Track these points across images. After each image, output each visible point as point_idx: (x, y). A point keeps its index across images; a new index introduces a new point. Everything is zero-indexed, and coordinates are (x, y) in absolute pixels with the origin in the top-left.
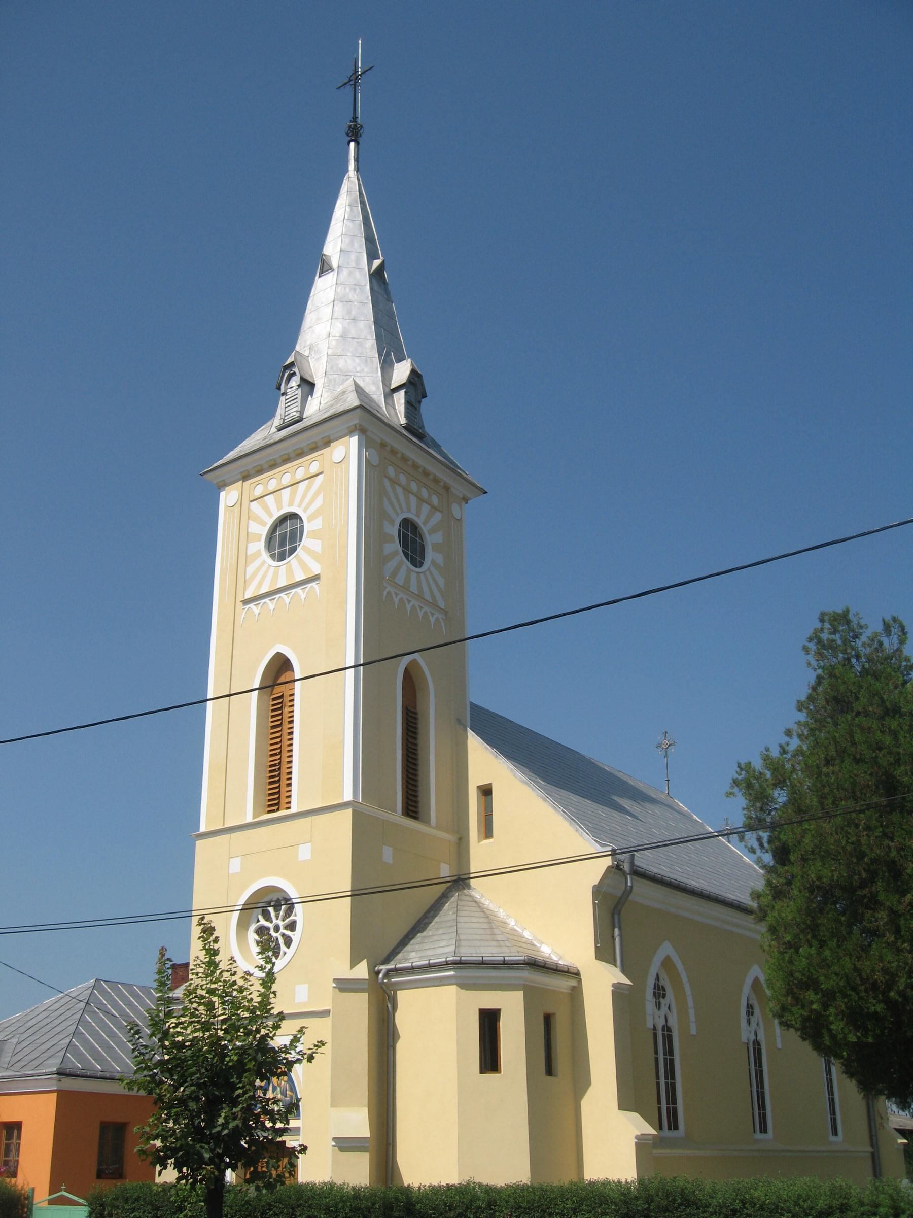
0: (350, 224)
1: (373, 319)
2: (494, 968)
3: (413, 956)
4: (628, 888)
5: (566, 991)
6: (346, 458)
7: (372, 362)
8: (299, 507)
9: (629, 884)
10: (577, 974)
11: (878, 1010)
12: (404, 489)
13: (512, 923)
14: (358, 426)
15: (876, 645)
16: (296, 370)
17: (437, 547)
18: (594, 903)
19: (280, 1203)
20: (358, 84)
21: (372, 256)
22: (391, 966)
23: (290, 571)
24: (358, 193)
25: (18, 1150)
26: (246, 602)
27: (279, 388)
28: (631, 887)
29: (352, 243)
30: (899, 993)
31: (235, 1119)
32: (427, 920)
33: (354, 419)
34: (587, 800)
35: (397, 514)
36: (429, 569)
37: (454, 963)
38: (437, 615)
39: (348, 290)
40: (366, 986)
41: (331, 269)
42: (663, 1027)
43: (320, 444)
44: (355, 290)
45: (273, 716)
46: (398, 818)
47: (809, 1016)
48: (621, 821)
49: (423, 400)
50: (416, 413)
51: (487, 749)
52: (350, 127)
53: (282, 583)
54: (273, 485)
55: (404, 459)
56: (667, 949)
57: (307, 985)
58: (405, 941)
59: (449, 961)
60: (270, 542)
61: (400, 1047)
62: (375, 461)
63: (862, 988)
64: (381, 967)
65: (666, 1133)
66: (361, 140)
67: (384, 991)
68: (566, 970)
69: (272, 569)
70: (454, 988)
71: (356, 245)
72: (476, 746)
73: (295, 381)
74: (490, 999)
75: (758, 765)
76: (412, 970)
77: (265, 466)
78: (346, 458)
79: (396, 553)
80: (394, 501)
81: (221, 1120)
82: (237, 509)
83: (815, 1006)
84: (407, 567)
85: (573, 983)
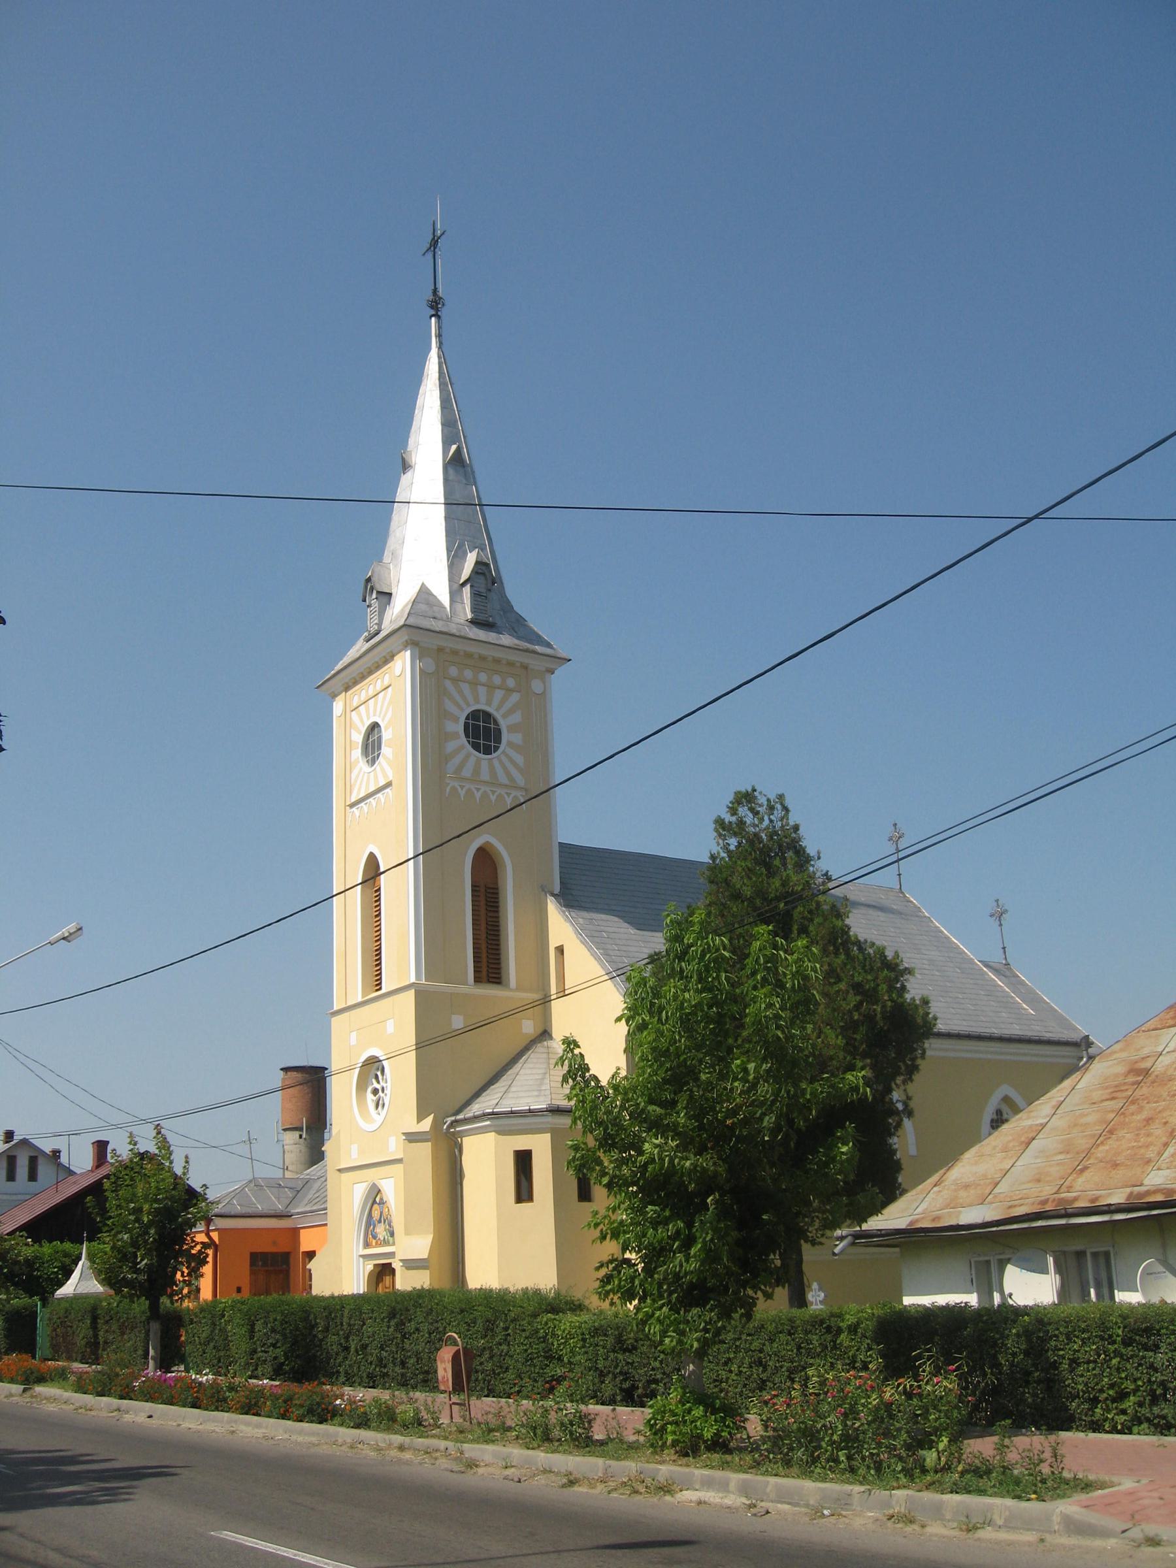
3: (476, 1108)
12: (470, 683)
26: (352, 805)
27: (364, 600)
36: (504, 752)
37: (489, 1114)
46: (469, 987)
53: (372, 789)
58: (477, 1095)
62: (431, 668)
66: (443, 313)
70: (491, 1136)
74: (522, 1142)
82: (343, 718)
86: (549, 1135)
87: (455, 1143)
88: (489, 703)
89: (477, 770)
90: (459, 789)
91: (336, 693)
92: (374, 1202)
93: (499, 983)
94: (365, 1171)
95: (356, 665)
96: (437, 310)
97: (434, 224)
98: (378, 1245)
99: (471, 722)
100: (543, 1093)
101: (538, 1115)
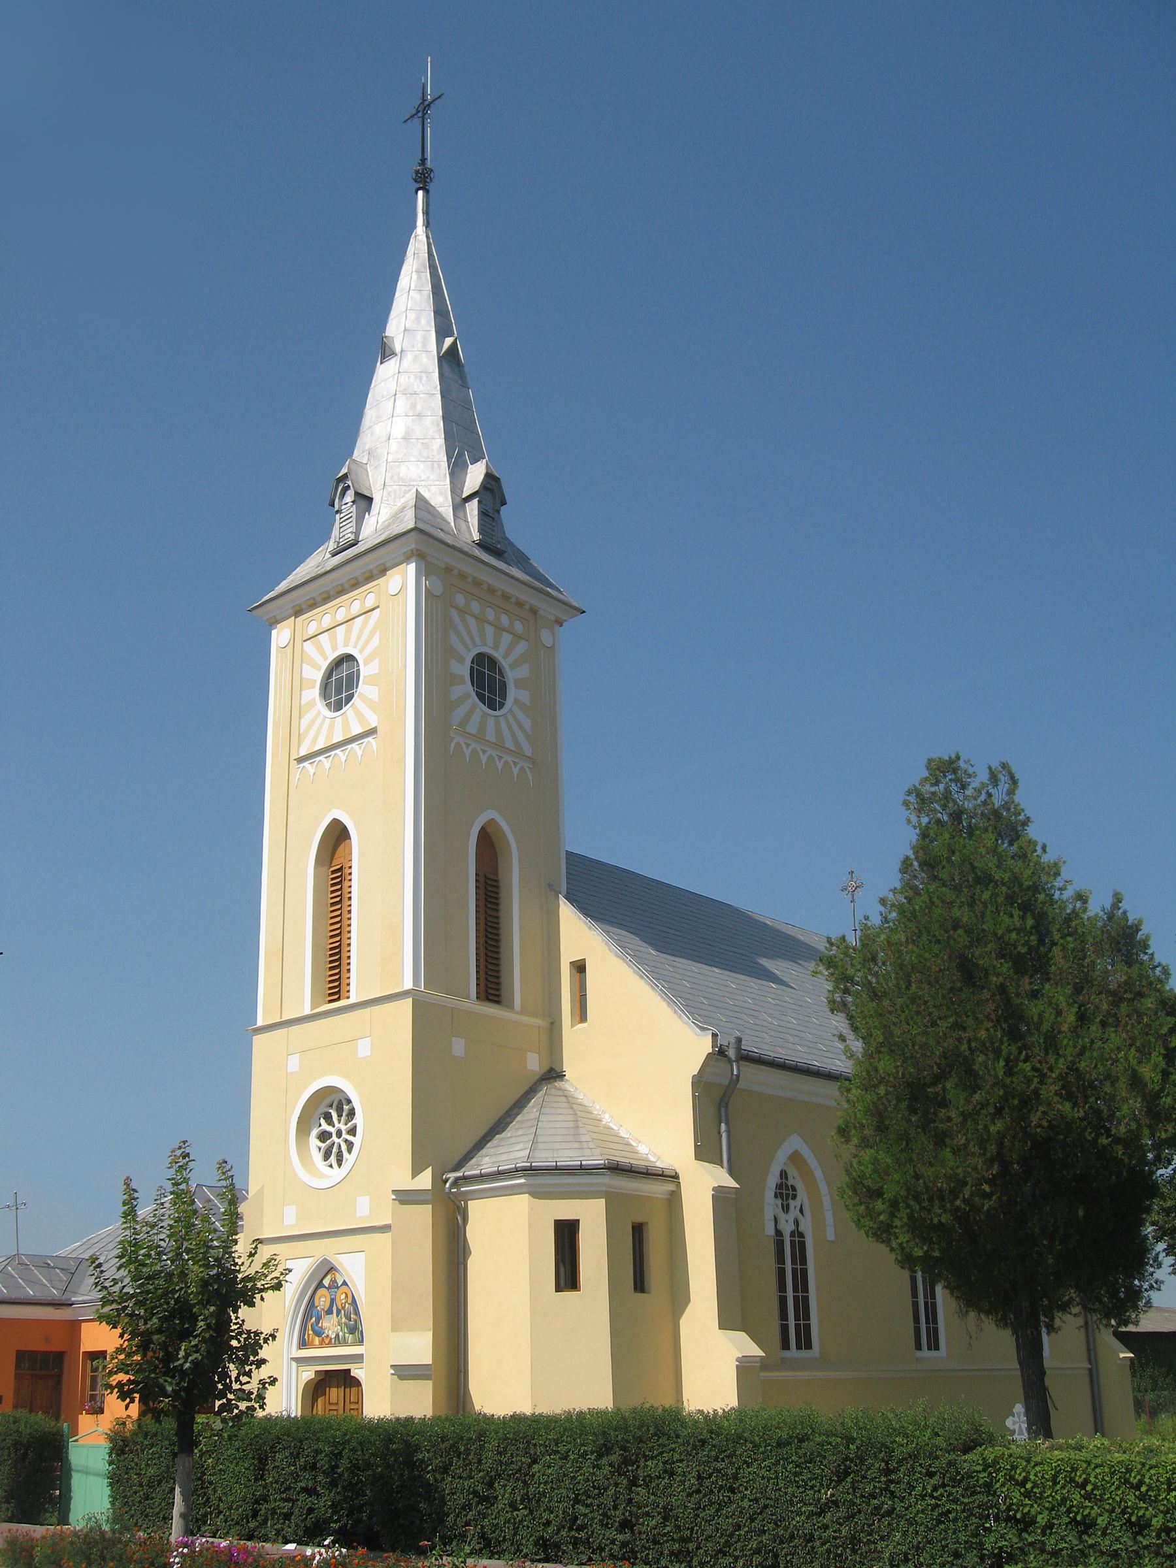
1: (441, 414)
2: (570, 1174)
3: (486, 1162)
4: (734, 1077)
5: (663, 1196)
6: (403, 587)
7: (439, 467)
8: (355, 647)
9: (735, 1073)
10: (676, 1177)
11: (943, 1221)
13: (606, 1118)
14: (414, 552)
15: (983, 797)
16: (350, 483)
17: (521, 684)
18: (693, 1095)
19: (289, 1436)
20: (426, 116)
21: (442, 332)
22: (459, 1174)
23: (346, 724)
24: (427, 255)
26: (301, 760)
28: (738, 1076)
29: (418, 319)
33: (411, 544)
34: (715, 969)
37: (525, 1169)
39: (412, 379)
40: (429, 1197)
41: (393, 354)
42: (792, 1234)
45: (332, 892)
46: (472, 1004)
48: (759, 992)
49: (502, 508)
50: (494, 524)
51: (580, 919)
52: (417, 172)
54: (327, 621)
55: (477, 583)
56: (795, 1143)
57: (368, 1197)
59: (519, 1167)
60: (325, 688)
62: (439, 591)
63: (926, 1197)
65: (793, 1352)
66: (431, 187)
67: (453, 1201)
68: (661, 1173)
69: (328, 721)
70: (525, 1197)
71: (423, 321)
72: (567, 914)
73: (349, 497)
74: (566, 1209)
76: (481, 1178)
77: (319, 599)
79: (467, 696)
80: (464, 633)
81: (182, 1354)
82: (289, 650)
84: (482, 711)
85: (671, 1187)
87: (458, 1207)
89: (482, 728)
91: (278, 618)
92: (320, 1285)
94: (310, 1243)
95: (366, 559)
98: (322, 1345)
99: (475, 667)
100: (585, 1145)
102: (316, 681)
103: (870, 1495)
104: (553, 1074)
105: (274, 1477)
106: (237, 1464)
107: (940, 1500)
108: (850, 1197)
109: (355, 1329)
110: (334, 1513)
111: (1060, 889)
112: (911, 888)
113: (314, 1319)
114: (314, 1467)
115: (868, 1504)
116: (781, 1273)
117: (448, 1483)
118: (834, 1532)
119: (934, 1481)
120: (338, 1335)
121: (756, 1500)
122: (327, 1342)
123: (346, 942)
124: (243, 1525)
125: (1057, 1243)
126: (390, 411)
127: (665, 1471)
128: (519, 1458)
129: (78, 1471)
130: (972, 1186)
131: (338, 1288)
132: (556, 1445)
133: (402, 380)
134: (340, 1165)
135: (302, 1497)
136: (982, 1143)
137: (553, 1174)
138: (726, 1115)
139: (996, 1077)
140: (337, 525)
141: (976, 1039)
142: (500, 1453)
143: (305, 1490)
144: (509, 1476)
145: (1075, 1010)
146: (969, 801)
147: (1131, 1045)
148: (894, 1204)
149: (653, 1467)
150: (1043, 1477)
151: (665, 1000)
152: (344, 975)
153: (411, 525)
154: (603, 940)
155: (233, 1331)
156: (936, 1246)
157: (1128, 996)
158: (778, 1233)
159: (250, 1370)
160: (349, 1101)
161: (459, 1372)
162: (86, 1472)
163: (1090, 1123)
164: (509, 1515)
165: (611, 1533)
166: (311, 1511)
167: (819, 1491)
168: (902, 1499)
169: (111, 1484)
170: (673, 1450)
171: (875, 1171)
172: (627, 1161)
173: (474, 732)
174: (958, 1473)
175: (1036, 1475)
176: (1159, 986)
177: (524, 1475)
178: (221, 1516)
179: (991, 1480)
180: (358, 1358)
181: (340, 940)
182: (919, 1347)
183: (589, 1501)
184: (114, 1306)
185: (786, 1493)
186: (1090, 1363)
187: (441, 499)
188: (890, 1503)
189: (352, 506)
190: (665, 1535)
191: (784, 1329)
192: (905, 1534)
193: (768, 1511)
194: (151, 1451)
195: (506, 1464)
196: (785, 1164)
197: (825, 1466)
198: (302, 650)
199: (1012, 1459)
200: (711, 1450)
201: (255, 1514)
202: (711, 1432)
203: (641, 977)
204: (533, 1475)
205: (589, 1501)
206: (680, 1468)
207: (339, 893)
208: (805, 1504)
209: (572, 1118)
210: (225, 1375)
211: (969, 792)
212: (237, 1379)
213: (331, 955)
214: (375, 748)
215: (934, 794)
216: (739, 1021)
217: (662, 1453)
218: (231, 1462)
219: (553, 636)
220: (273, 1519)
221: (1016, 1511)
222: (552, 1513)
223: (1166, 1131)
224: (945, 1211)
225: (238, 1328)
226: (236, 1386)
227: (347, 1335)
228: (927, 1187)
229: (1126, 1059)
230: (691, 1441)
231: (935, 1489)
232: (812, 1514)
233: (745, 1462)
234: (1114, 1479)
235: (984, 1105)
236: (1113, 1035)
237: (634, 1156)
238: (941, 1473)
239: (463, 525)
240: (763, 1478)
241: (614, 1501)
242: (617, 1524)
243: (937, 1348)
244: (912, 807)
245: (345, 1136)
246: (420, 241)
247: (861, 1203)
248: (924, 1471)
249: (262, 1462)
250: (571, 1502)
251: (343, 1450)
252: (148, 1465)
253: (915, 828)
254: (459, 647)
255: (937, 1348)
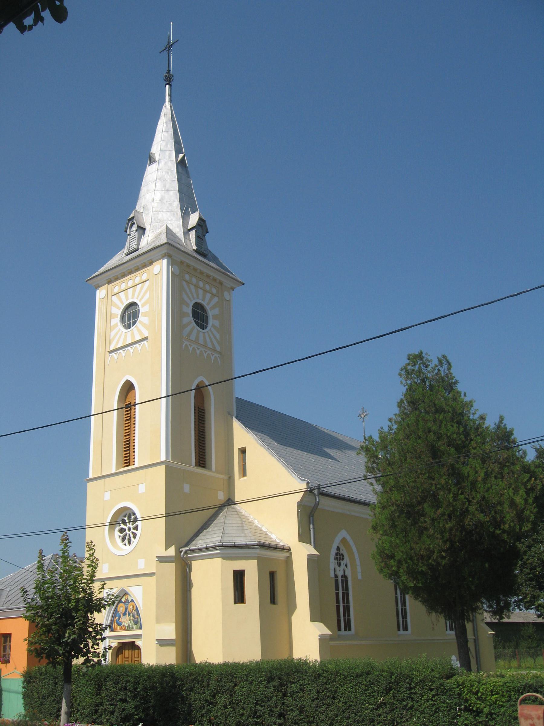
0: (166, 134)
2: (241, 548)
3: (200, 542)
6: (161, 271)
7: (177, 214)
8: (137, 299)
9: (317, 501)
10: (289, 550)
11: (424, 569)
12: (195, 286)
13: (256, 522)
15: (436, 371)
16: (134, 221)
17: (215, 317)
18: (298, 511)
19: (113, 674)
20: (170, 50)
21: (178, 151)
22: (188, 548)
23: (133, 335)
25: (10, 649)
26: (111, 352)
27: (126, 232)
29: (166, 145)
30: (434, 560)
31: (74, 634)
32: (210, 523)
33: (165, 250)
35: (191, 301)
36: (210, 330)
37: (219, 546)
38: (215, 355)
39: (164, 173)
40: (174, 560)
41: (155, 161)
42: (342, 577)
43: (113, 279)
44: (168, 173)
45: (126, 414)
46: (193, 468)
47: (392, 573)
51: (243, 428)
52: (166, 76)
53: (129, 341)
54: (123, 287)
55: (195, 269)
56: (343, 534)
60: (123, 318)
61: (193, 590)
62: (177, 272)
63: (415, 558)
64: (183, 549)
65: (343, 632)
66: (172, 83)
67: (185, 562)
70: (220, 559)
71: (169, 146)
72: (238, 427)
73: (134, 228)
74: (239, 565)
75: (376, 438)
76: (198, 550)
78: (161, 271)
79: (191, 322)
81: (67, 635)
82: (105, 300)
83: (394, 568)
85: (287, 554)
86: (256, 561)
88: (204, 300)
89: (197, 337)
90: (189, 346)
91: (100, 285)
93: (204, 467)
95: (126, 265)
96: (170, 81)
97: (169, 37)
98: (121, 630)
101: (251, 548)
102: (118, 314)
103: (402, 699)
104: (230, 502)
105: (105, 694)
106: (87, 687)
107: (436, 702)
108: (378, 559)
109: (138, 623)
110: (136, 711)
111: (473, 414)
112: (404, 414)
113: (117, 618)
114: (125, 689)
115: (401, 704)
116: (337, 595)
117: (193, 696)
118: (384, 717)
119: (433, 693)
120: (129, 625)
121: (346, 703)
122: (123, 628)
123: (132, 438)
124: (90, 717)
125: (476, 580)
126: (154, 188)
127: (301, 689)
128: (228, 684)
129: (5, 691)
130: (437, 553)
131: (129, 603)
132: (247, 677)
133: (159, 173)
134: (130, 544)
135: (119, 703)
136: (442, 533)
137: (233, 549)
138: (313, 521)
139: (449, 501)
140: (128, 241)
141: (439, 484)
142: (219, 681)
143: (121, 700)
144: (223, 692)
145: (484, 470)
146: (430, 373)
147: (509, 487)
148: (400, 562)
149: (295, 687)
150: (486, 690)
151: (284, 466)
152: (132, 454)
153: (165, 241)
154: (254, 438)
155: (89, 624)
156: (420, 582)
157: (507, 464)
158: (336, 576)
159: (98, 642)
160: (134, 514)
161: (187, 642)
162: (9, 691)
163: (491, 524)
164: (223, 711)
165: (274, 719)
166: (124, 710)
167: (377, 698)
168: (417, 701)
169: (24, 698)
170: (305, 679)
171: (391, 546)
172: (267, 542)
173: (194, 339)
174: (445, 689)
175: (483, 689)
176: (522, 460)
177: (231, 693)
178: (79, 713)
179: (461, 692)
180: (139, 636)
181: (130, 438)
182: (399, 630)
183: (263, 704)
184: (33, 612)
185: (360, 699)
186: (475, 636)
187: (178, 230)
188: (411, 703)
189: (136, 232)
190: (300, 720)
191: (339, 621)
192: (419, 718)
193: (352, 708)
194: (44, 682)
195: (222, 686)
196: (339, 544)
197: (380, 686)
198: (111, 300)
199: (471, 682)
200: (323, 679)
201: (96, 711)
202: (323, 670)
203: (273, 456)
204: (235, 692)
205: (263, 704)
206: (308, 688)
207: (129, 415)
208: (370, 704)
209: (240, 522)
210: (87, 645)
211: (429, 369)
212: (92, 647)
213: (125, 445)
214: (147, 346)
215: (413, 370)
216: (317, 477)
217: (299, 681)
218: (84, 687)
219: (230, 295)
220: (105, 714)
221: (473, 707)
222: (244, 710)
223: (527, 527)
224: (424, 565)
225: (92, 622)
226: (92, 650)
227: (133, 625)
228: (416, 554)
229: (508, 494)
230: (314, 675)
231: (434, 696)
232: (373, 709)
233: (340, 685)
234: (465, 690)
235: (443, 515)
236: (501, 482)
237: (270, 540)
238: (436, 689)
239: (188, 242)
240: (349, 692)
241: (275, 704)
242: (277, 715)
243: (407, 630)
244: (403, 376)
245: (132, 530)
246: (167, 109)
247: (383, 562)
248: (428, 688)
249: (99, 687)
250: (254, 705)
251: (139, 680)
252: (42, 688)
253: (405, 386)
254: (186, 298)
255: (407, 630)
